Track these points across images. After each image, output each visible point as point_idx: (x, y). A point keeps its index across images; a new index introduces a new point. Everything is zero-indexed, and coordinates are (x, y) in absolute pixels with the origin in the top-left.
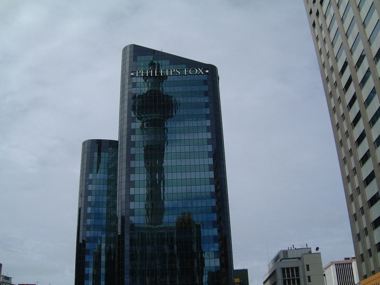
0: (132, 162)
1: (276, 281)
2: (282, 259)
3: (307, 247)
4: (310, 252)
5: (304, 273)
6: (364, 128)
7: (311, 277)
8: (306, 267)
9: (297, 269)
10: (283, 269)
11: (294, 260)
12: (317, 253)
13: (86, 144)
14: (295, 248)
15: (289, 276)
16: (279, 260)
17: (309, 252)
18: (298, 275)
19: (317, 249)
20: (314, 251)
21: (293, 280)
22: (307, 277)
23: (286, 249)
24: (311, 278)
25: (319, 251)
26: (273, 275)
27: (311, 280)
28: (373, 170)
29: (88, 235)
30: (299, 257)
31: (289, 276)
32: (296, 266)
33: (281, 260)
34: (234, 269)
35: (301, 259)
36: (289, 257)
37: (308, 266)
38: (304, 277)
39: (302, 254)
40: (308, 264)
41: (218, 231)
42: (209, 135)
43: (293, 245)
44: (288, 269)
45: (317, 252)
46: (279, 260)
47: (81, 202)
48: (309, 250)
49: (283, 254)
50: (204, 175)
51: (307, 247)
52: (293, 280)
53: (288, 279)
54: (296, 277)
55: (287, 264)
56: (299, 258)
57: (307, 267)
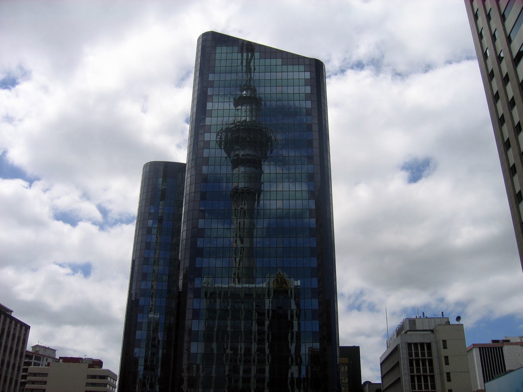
0: (198, 259)
1: (400, 377)
2: (408, 331)
3: (443, 316)
4: (448, 322)
5: (438, 352)
6: (520, 189)
7: (449, 357)
8: (445, 376)
9: (429, 345)
10: (409, 345)
11: (425, 332)
12: (458, 325)
13: (148, 167)
14: (426, 317)
15: (418, 371)
16: (404, 332)
17: (446, 323)
18: (430, 354)
19: (458, 318)
20: (453, 321)
21: (424, 361)
22: (446, 374)
23: (414, 317)
24: (450, 359)
25: (461, 322)
26: (394, 353)
27: (450, 362)
28: (519, 121)
29: (143, 287)
30: (431, 329)
31: (418, 371)
32: (428, 342)
33: (406, 333)
34: (340, 345)
35: (434, 331)
36: (417, 329)
37: (444, 342)
38: (441, 374)
39: (436, 325)
40: (445, 339)
41: (319, 281)
42: (308, 89)
43: (423, 313)
44: (416, 345)
45: (457, 323)
46: (404, 332)
47: (136, 243)
48: (445, 320)
49: (410, 324)
50: (304, 90)
51: (443, 316)
52: (424, 361)
53: (415, 359)
54: (430, 373)
55: (417, 338)
56: (432, 331)
57: (445, 360)
